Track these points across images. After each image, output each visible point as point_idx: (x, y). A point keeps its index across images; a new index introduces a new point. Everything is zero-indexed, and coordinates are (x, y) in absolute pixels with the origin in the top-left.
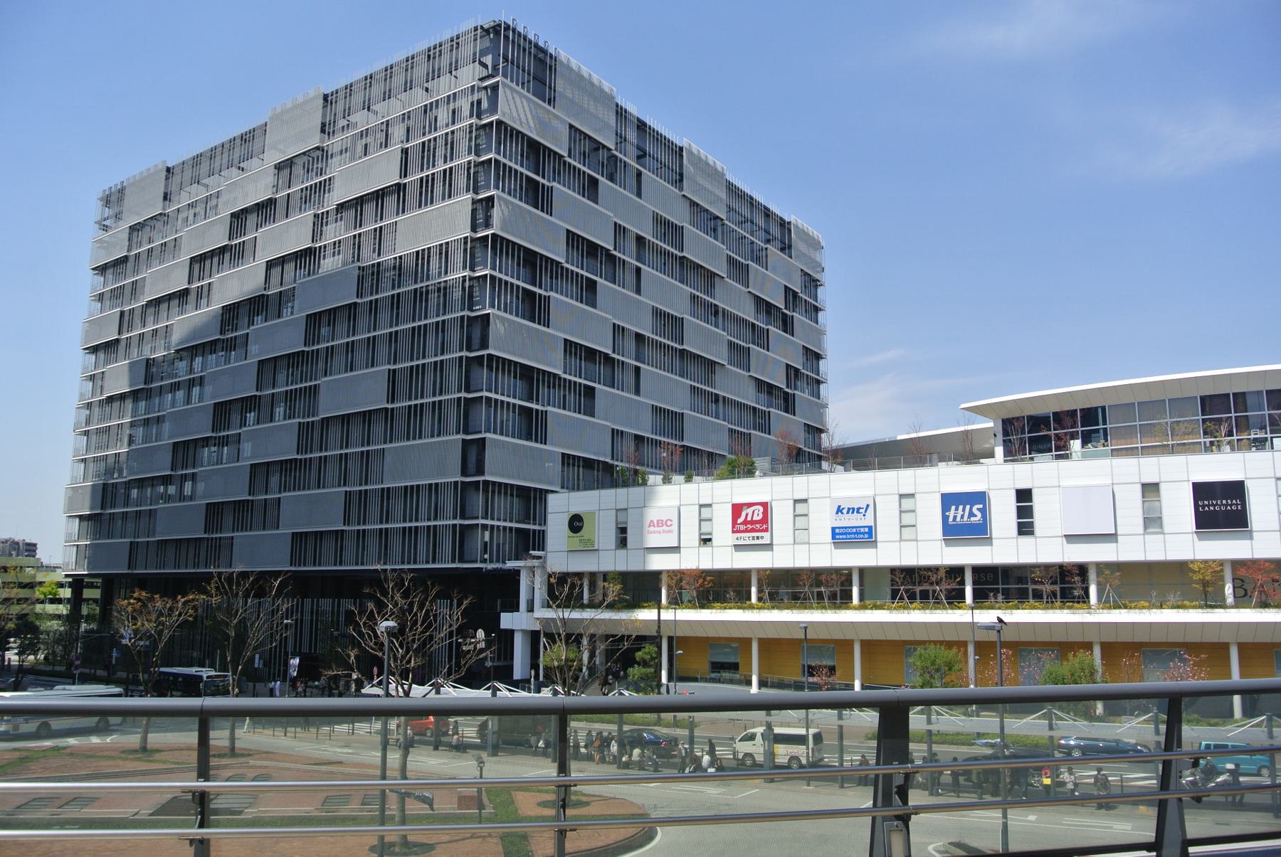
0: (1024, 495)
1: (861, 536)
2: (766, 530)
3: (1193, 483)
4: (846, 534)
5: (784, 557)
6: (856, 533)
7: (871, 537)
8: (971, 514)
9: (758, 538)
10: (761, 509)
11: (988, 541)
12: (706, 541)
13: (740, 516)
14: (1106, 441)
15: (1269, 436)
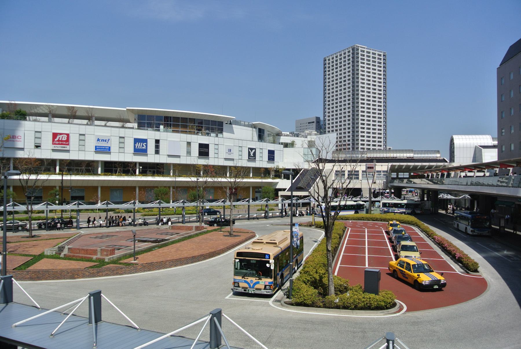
0: (157, 141)
1: (106, 150)
2: (68, 145)
3: (199, 144)
4: (100, 149)
5: (74, 155)
6: (104, 149)
7: (109, 150)
8: (143, 146)
9: (64, 147)
10: (66, 136)
11: (147, 155)
12: (37, 147)
13: (56, 138)
14: (171, 127)
15: (210, 132)
